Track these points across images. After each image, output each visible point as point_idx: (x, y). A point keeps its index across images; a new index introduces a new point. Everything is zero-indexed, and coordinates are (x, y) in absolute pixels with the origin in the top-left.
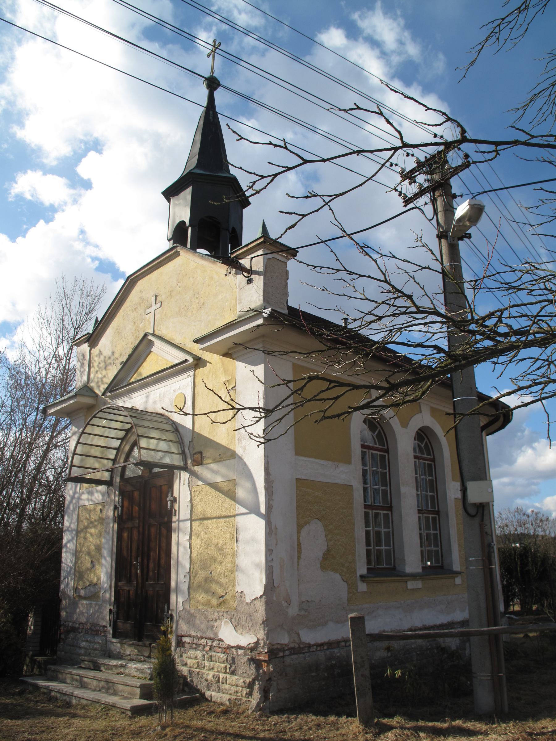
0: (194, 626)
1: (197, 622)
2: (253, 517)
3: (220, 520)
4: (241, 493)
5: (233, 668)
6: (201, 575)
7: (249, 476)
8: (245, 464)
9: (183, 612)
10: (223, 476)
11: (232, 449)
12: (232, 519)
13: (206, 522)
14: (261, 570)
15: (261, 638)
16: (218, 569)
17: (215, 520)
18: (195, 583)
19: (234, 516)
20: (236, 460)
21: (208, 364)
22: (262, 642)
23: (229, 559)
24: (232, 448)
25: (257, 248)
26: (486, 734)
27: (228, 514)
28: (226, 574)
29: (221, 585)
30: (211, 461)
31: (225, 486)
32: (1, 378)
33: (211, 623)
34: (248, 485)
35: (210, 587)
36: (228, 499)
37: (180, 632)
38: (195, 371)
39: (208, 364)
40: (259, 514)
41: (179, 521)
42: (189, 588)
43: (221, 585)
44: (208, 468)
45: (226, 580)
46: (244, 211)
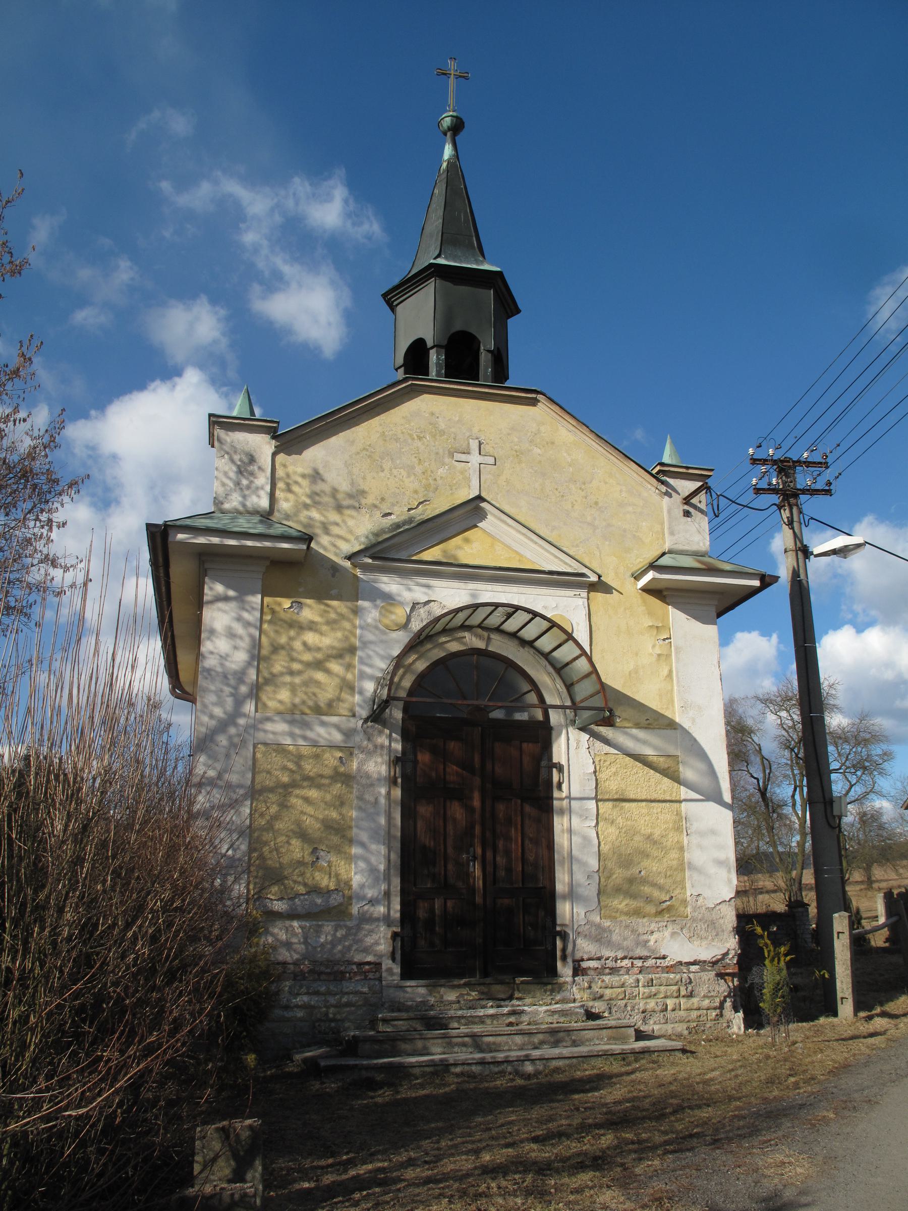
0: (609, 944)
1: (615, 937)
2: (712, 806)
3: (653, 804)
4: (688, 773)
5: (690, 988)
6: (619, 875)
7: (702, 755)
8: (695, 740)
9: (587, 927)
10: (655, 748)
11: (670, 716)
12: (676, 805)
13: (624, 804)
14: (730, 869)
15: (733, 947)
16: (651, 867)
17: (644, 804)
18: (609, 886)
19: (680, 802)
20: (678, 732)
21: (870, 936)
22: (732, 953)
23: (674, 855)
24: (668, 714)
25: (697, 477)
26: (409, 510)
27: (668, 798)
28: (668, 873)
29: (661, 888)
30: (630, 725)
31: (662, 762)
32: (0, 463)
33: (645, 937)
34: (701, 766)
35: (253, 959)
36: (666, 780)
37: (578, 956)
38: (588, 593)
39: (868, 936)
40: (720, 801)
41: (569, 797)
42: (599, 894)
43: (661, 888)
44: (850, 883)
45: (669, 881)
46: (739, 635)
